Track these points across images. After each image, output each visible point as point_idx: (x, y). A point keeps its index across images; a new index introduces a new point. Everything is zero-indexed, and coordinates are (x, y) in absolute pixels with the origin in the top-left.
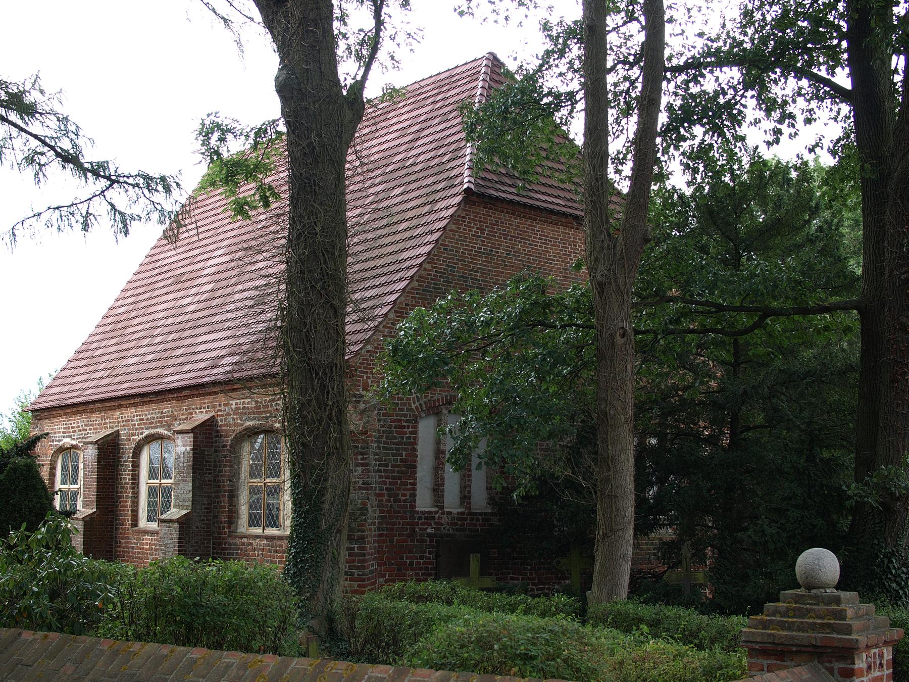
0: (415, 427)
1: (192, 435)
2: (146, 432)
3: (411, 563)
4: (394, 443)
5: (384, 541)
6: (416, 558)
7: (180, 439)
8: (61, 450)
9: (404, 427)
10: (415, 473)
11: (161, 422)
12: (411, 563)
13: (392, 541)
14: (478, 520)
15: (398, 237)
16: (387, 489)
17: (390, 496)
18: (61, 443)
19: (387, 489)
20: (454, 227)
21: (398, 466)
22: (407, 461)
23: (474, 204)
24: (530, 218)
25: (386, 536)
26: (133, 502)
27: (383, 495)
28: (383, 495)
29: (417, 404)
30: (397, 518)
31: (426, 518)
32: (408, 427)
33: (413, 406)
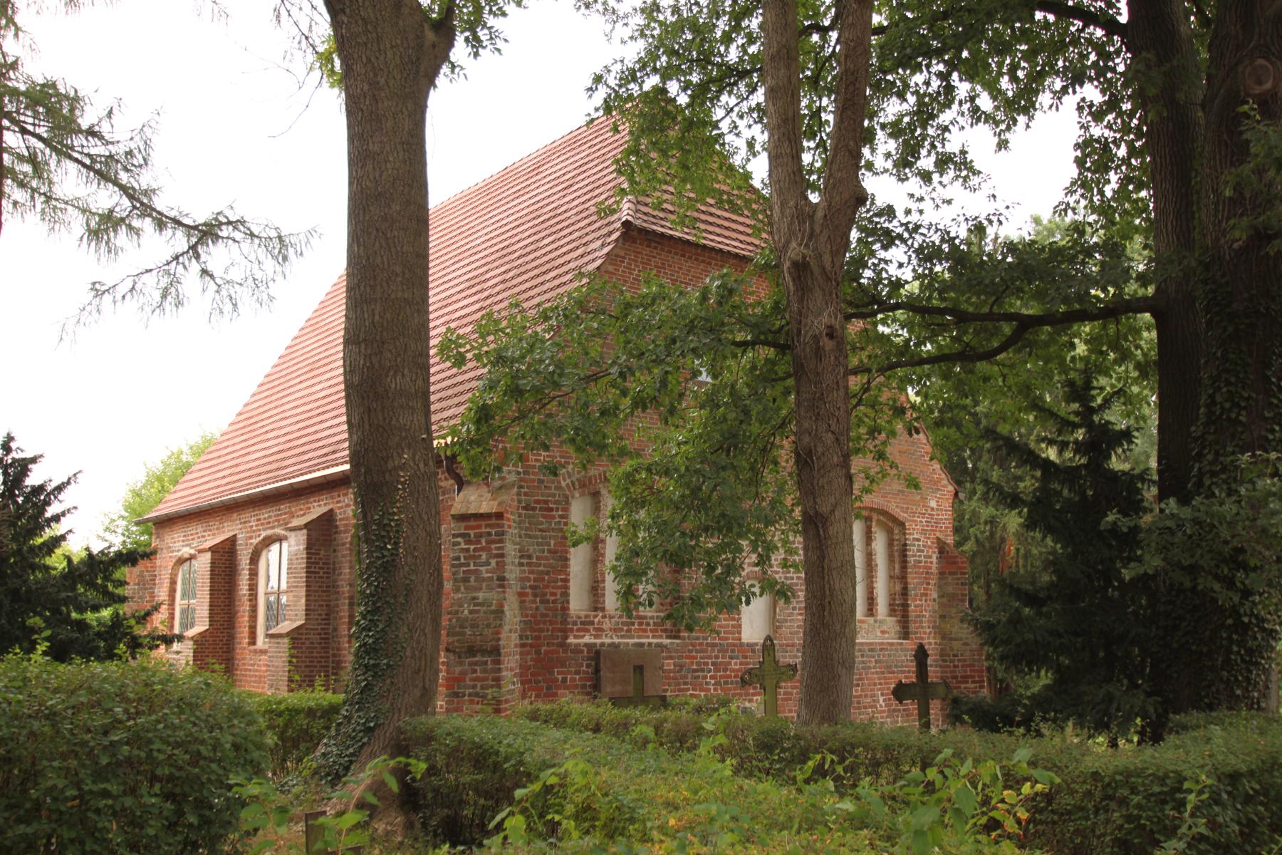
0: (566, 509)
1: (305, 531)
2: (264, 534)
3: (564, 680)
4: (541, 530)
5: (528, 653)
6: (569, 673)
7: (293, 537)
8: (181, 561)
9: (551, 510)
10: (567, 566)
11: (278, 521)
12: (564, 680)
13: (538, 653)
14: (648, 624)
15: (548, 285)
16: (531, 587)
17: (535, 595)
18: (179, 554)
19: (531, 587)
20: (611, 268)
21: (547, 559)
22: (556, 552)
23: (634, 242)
24: (703, 261)
25: (531, 646)
26: (250, 617)
27: (527, 595)
28: (527, 595)
29: (568, 481)
30: (545, 623)
31: (582, 623)
32: (557, 510)
33: (563, 484)
